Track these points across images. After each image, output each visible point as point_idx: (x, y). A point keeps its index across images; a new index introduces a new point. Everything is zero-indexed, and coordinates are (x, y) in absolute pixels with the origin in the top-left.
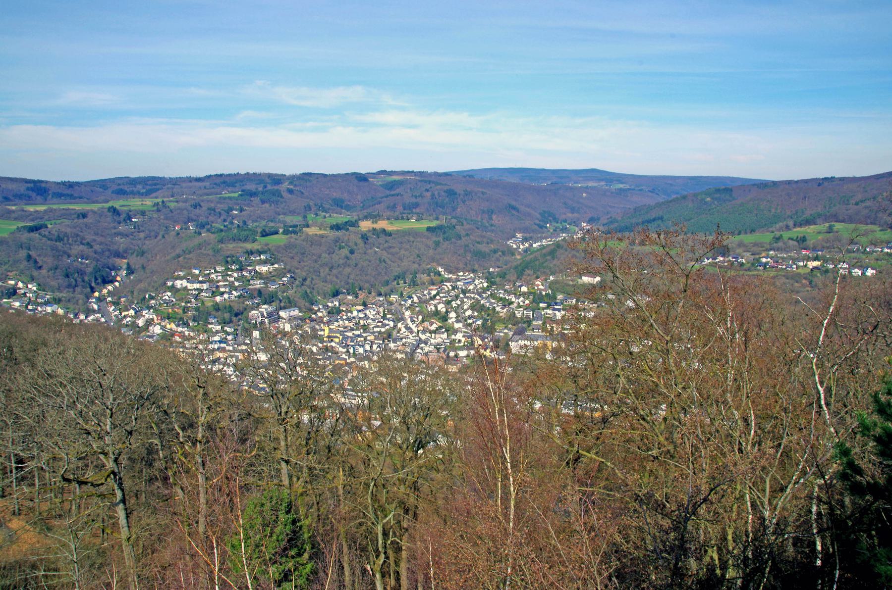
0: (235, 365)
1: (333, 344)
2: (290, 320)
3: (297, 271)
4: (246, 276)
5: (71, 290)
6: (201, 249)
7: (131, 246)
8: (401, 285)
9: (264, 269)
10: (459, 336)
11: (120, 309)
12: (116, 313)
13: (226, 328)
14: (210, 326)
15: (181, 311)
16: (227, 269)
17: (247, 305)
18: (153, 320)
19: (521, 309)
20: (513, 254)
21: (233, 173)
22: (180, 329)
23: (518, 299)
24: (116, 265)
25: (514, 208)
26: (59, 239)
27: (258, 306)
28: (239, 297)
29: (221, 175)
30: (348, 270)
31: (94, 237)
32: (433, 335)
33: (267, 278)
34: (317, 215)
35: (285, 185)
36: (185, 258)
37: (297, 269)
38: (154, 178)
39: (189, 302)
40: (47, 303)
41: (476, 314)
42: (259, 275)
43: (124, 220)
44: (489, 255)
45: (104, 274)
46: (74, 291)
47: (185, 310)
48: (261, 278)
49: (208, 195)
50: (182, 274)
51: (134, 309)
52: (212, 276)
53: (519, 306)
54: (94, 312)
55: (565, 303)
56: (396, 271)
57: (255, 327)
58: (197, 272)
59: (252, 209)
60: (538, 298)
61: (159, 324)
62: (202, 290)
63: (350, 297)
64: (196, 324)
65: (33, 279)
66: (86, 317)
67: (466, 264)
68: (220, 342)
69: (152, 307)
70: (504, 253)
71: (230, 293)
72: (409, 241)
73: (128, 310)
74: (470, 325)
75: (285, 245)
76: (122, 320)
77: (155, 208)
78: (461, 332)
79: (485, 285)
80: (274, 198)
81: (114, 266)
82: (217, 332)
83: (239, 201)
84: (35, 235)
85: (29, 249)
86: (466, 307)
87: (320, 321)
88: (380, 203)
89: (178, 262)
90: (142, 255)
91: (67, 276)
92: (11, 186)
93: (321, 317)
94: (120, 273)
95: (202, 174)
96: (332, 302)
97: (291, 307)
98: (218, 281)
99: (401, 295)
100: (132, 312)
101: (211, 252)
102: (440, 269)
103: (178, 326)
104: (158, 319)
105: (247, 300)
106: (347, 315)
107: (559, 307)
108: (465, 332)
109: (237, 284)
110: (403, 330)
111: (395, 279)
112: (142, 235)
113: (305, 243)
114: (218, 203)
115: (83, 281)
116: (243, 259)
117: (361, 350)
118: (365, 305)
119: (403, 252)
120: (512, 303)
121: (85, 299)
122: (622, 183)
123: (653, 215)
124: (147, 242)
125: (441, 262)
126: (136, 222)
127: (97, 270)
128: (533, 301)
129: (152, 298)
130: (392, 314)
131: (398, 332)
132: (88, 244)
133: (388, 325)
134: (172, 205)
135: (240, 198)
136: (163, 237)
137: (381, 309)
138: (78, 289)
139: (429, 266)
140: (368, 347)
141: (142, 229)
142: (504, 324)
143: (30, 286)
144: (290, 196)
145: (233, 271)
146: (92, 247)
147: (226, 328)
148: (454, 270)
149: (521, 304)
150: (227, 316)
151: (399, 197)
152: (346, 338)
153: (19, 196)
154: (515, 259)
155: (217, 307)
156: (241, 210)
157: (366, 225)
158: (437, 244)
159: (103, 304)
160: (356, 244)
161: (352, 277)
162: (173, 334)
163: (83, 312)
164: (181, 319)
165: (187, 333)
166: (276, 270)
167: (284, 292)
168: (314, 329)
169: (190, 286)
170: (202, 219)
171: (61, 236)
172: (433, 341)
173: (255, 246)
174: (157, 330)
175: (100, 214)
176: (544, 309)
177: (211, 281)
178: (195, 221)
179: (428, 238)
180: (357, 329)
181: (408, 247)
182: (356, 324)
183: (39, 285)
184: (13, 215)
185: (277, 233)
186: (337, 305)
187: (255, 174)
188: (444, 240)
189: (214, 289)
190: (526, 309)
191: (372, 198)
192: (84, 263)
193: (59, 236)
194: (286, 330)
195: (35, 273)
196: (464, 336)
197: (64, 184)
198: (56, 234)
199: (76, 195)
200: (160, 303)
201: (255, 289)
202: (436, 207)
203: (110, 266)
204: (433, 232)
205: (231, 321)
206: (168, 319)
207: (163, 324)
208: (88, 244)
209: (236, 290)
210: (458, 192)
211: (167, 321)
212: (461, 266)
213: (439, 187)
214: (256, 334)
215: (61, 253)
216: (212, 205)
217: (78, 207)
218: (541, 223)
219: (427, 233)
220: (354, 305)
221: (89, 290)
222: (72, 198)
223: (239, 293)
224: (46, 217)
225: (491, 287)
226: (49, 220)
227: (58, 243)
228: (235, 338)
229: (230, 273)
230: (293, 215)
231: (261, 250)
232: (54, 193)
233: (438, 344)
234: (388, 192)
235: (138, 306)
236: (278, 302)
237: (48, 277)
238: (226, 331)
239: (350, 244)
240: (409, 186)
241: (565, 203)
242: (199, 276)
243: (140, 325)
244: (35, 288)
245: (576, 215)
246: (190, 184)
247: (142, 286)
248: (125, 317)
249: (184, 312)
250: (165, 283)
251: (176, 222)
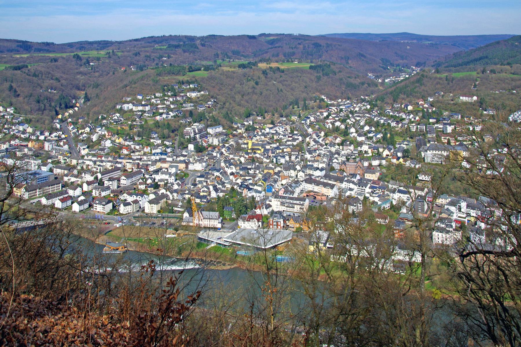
0: (176, 175)
1: (258, 155)
2: (217, 135)
3: (218, 97)
4: (179, 101)
5: (40, 112)
6: (143, 80)
7: (89, 82)
8: (295, 109)
9: (194, 95)
10: (365, 148)
11: (77, 128)
12: (74, 131)
13: (165, 142)
14: (152, 141)
15: (127, 128)
16: (165, 95)
17: (181, 123)
18: (105, 135)
20: (377, 86)
21: (160, 35)
22: (127, 143)
24: (76, 95)
26: (35, 75)
27: (190, 124)
28: (174, 117)
29: (152, 37)
30: (255, 97)
31: (61, 75)
32: (341, 147)
33: (196, 102)
34: (223, 60)
35: (198, 42)
36: (131, 87)
37: (218, 95)
38: (104, 41)
39: (134, 121)
40: (20, 123)
41: (373, 129)
42: (190, 100)
43: (85, 64)
45: (67, 101)
46: (43, 113)
47: (131, 127)
48: (191, 102)
49: (144, 47)
50: (129, 99)
51: (89, 127)
52: (153, 100)
54: (57, 130)
55: (452, 119)
56: (291, 98)
57: (190, 141)
58: (140, 97)
59: (177, 56)
60: (426, 116)
61: (110, 139)
62: (145, 112)
63: (259, 118)
64: (140, 139)
65: (11, 105)
66: (50, 134)
67: (342, 93)
68: (161, 154)
69: (104, 125)
70: (369, 85)
71: (168, 113)
72: (297, 77)
73: (84, 128)
74: (371, 138)
75: (208, 77)
76: (79, 136)
77: (108, 56)
78: (366, 144)
80: (192, 49)
81: (75, 96)
82: (158, 145)
83: (167, 51)
84: (19, 72)
85: (12, 82)
86: (362, 124)
87: (241, 137)
88: (267, 52)
89: (126, 90)
90: (97, 87)
91: (38, 102)
92: (6, 44)
93: (240, 133)
94: (79, 101)
95: (140, 37)
96: (247, 122)
97: (216, 125)
98: (158, 105)
99: (299, 117)
100: (88, 129)
101: (151, 82)
102: (323, 97)
103: (126, 140)
104: (109, 135)
105: (181, 119)
106: (261, 132)
109: (172, 106)
110: (312, 143)
111: (291, 105)
112: (97, 74)
113: (222, 76)
114: (152, 52)
115: (50, 106)
116: (177, 87)
117: (282, 161)
118: (272, 123)
119: (294, 84)
121: (51, 120)
122: (429, 41)
124: (100, 79)
125: (323, 91)
126: (92, 65)
127: (62, 98)
128: (423, 117)
129: (104, 118)
130: (297, 131)
131: (308, 145)
132: (57, 79)
133: (298, 139)
134: (119, 54)
135: (168, 49)
136: (114, 74)
137: (288, 127)
138: (46, 112)
139: (314, 95)
140: (287, 158)
141: (97, 70)
142: (402, 137)
143: (8, 110)
144: (204, 48)
145: (169, 97)
146: (59, 81)
147: (165, 142)
149: (413, 120)
150: (166, 131)
151: (280, 48)
152: (266, 150)
153: (10, 51)
155: (157, 124)
156: (169, 57)
157: (263, 66)
158: (319, 78)
159: (63, 124)
160: (259, 78)
161: (259, 102)
162: (121, 147)
163: (48, 130)
164: (128, 134)
165: (133, 146)
166: (202, 96)
167: (210, 113)
168: (237, 143)
169: (134, 108)
170: (141, 63)
171: (37, 73)
173: (185, 78)
174: (108, 144)
175: (68, 60)
176: (434, 124)
177: (152, 105)
178: (136, 64)
179: (311, 74)
180: (273, 143)
181: (297, 80)
182: (271, 138)
183: (16, 109)
184: (4, 60)
185: (200, 70)
186: (251, 124)
187: (176, 36)
188: (323, 75)
189: (154, 111)
190: (419, 124)
191: (260, 50)
192: (53, 93)
193: (35, 73)
194: (214, 144)
195: (14, 100)
197: (43, 43)
198: (33, 71)
199: (50, 49)
200: (111, 123)
201: (187, 110)
202: (306, 55)
203: (72, 95)
204: (315, 69)
205: (169, 137)
206: (117, 135)
207: (113, 139)
208: (57, 79)
209: (172, 111)
210: (322, 45)
211: (116, 136)
212: (338, 94)
213: (307, 42)
214: (191, 147)
215: (36, 85)
216: (148, 54)
217: (52, 55)
219: (309, 71)
220: (265, 124)
221: (54, 113)
222: (48, 51)
223: (175, 114)
224: (28, 61)
226: (30, 63)
227: (34, 78)
228: (173, 150)
229: (166, 98)
230: (206, 60)
231: (190, 81)
232: (35, 49)
234: (270, 46)
235: (92, 124)
236: (206, 120)
237: (24, 102)
238: (165, 144)
239: (255, 78)
240: (285, 42)
241: (396, 53)
242: (142, 100)
243: (94, 140)
244: (12, 112)
246: (131, 43)
247: (96, 109)
248: (82, 133)
249: (131, 129)
250: (115, 107)
251: (122, 65)
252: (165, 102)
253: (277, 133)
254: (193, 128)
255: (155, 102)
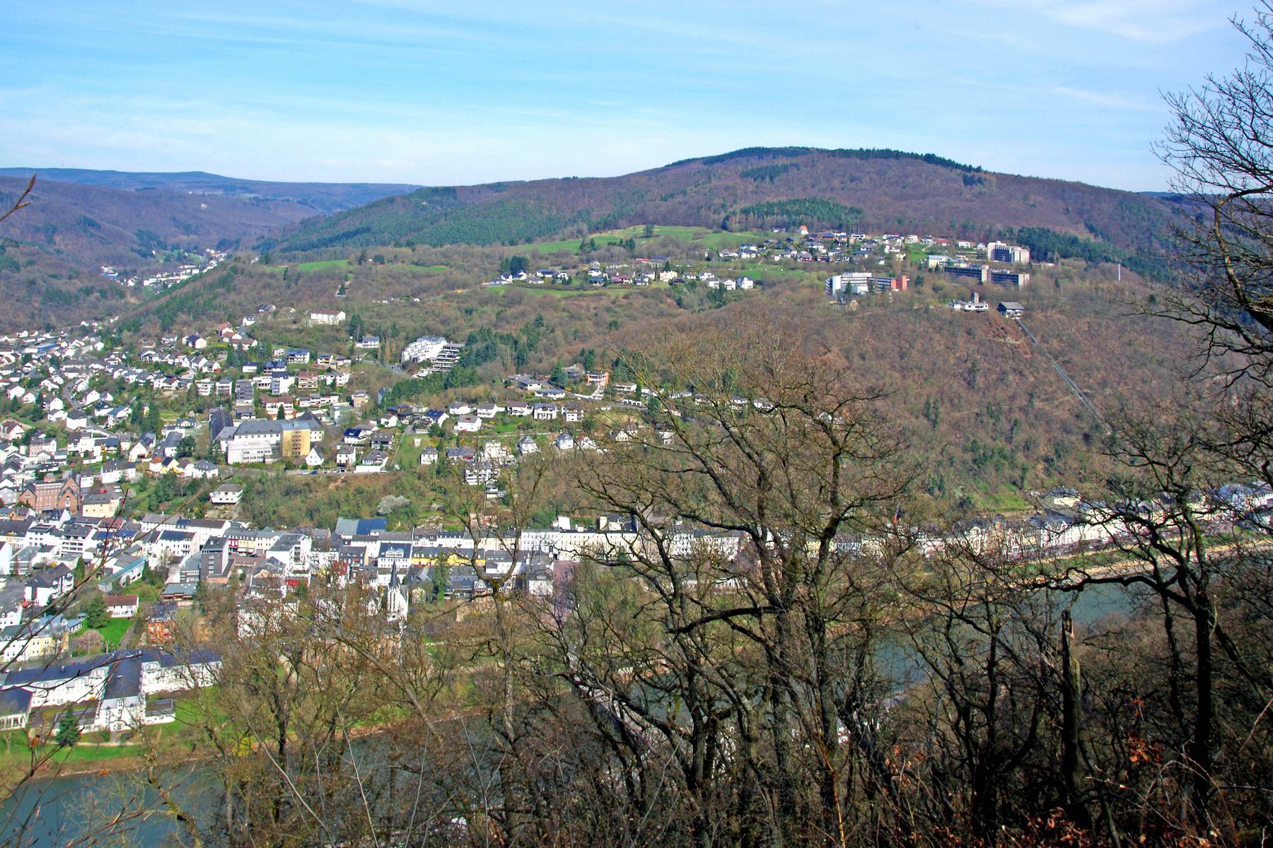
10: (86, 444)
19: (207, 380)
20: (122, 296)
23: (197, 361)
25: (92, 224)
41: (110, 398)
44: (77, 297)
53: (201, 375)
60: (236, 358)
67: (33, 316)
70: (104, 294)
78: (89, 435)
79: (100, 346)
107: (283, 370)
108: (95, 436)
120: (185, 370)
122: (251, 192)
123: (348, 226)
142: (178, 411)
148: (9, 329)
149: (205, 370)
154: (127, 303)
172: (27, 461)
176: (251, 376)
190: (218, 379)
196: (97, 443)
212: (22, 319)
218: (144, 249)
225: (112, 349)
233: (43, 466)
245: (193, 237)
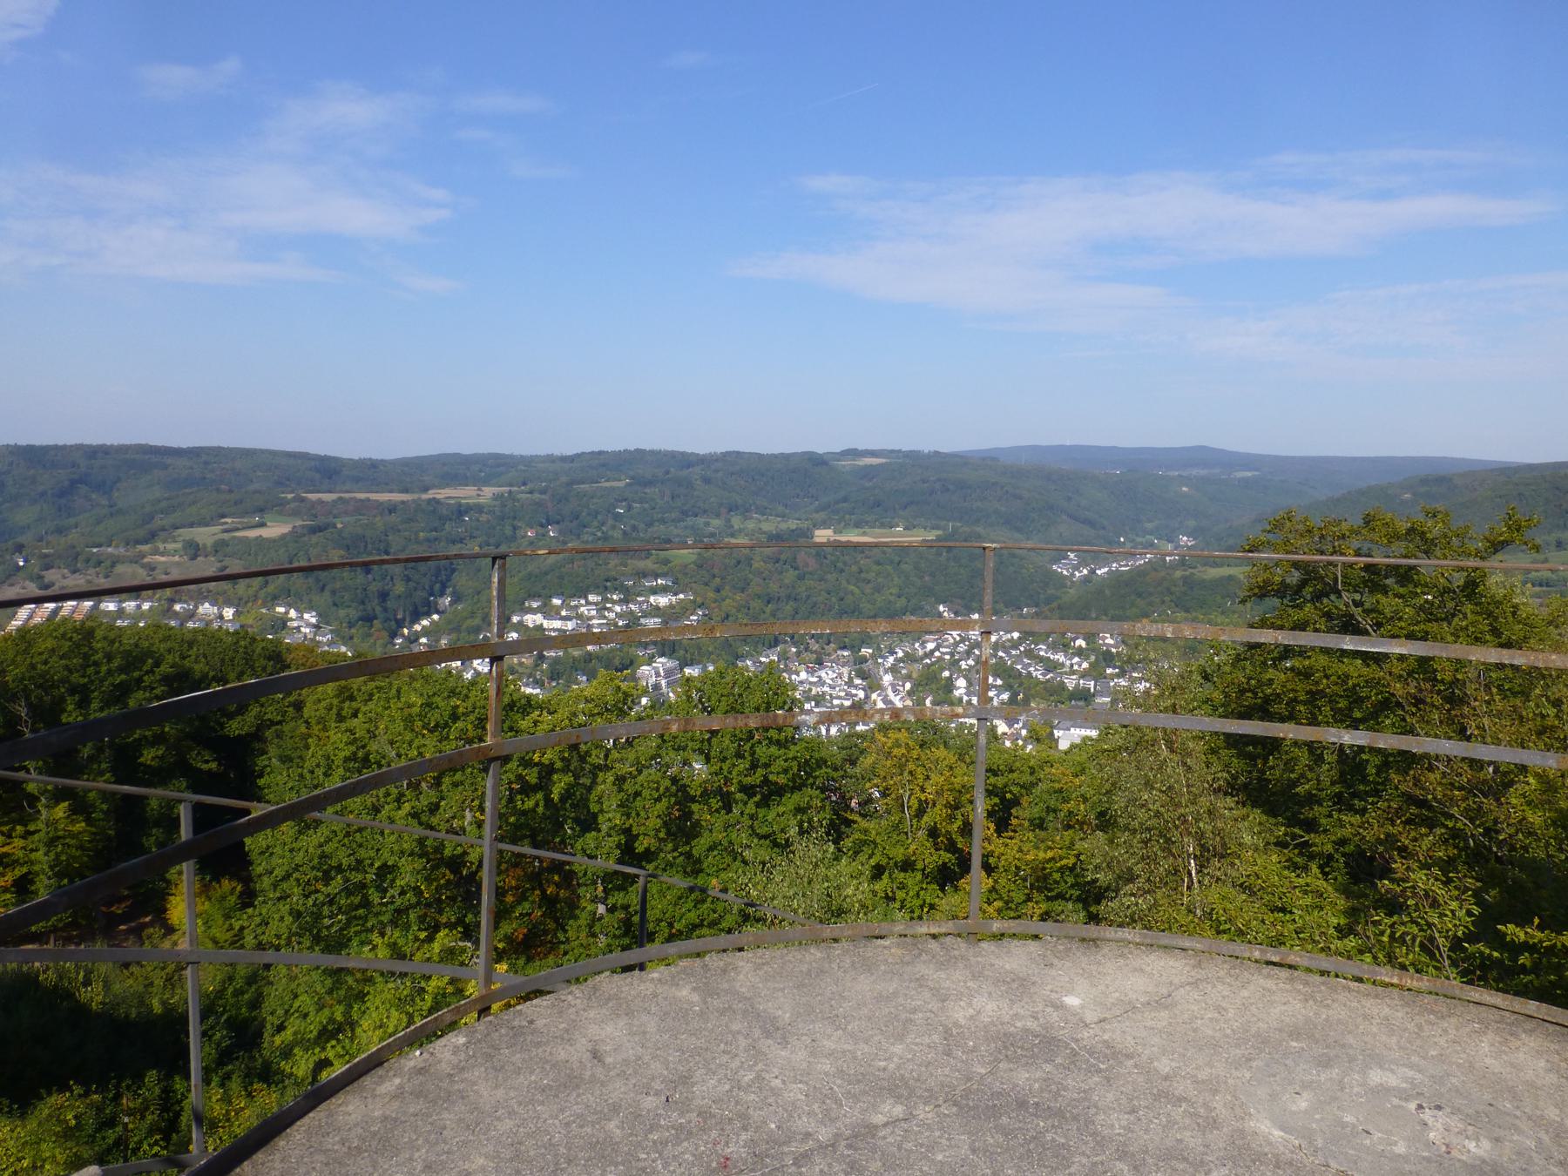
9: (663, 601)
16: (605, 600)
50: (535, 605)
143: (306, 616)
145: (614, 602)
149: (1076, 667)
169: (546, 624)
177: (580, 617)
229: (608, 605)
252: (606, 613)
253: (821, 682)
254: (654, 668)
255: (586, 612)
